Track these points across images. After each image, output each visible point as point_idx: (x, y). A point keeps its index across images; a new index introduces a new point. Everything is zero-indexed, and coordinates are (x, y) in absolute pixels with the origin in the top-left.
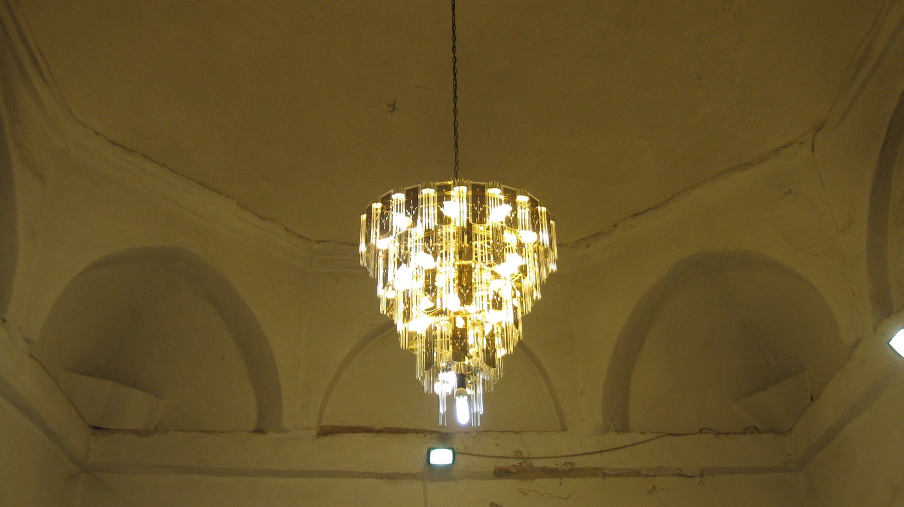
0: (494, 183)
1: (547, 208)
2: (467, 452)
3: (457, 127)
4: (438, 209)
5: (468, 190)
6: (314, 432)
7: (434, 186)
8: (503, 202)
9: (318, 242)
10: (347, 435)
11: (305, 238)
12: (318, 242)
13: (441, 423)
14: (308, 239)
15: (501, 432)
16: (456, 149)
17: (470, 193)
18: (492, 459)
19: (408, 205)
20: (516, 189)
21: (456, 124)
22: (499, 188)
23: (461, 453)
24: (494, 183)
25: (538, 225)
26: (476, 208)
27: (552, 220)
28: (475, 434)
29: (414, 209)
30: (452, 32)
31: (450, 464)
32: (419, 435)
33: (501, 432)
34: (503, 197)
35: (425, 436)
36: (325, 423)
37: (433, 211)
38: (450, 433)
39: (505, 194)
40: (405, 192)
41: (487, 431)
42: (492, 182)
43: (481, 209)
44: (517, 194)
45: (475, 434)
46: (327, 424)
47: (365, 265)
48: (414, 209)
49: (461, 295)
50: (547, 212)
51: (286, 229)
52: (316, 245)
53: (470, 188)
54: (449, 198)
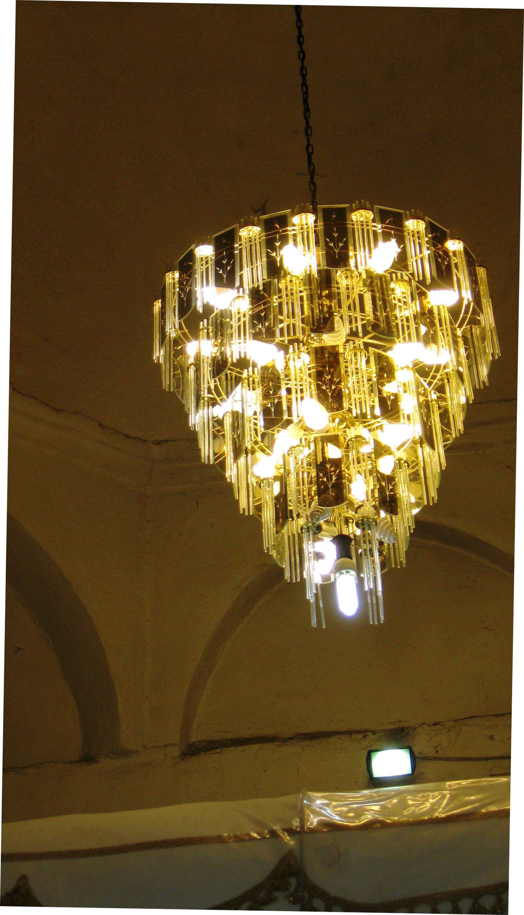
0: (360, 202)
1: (464, 242)
2: (441, 754)
3: (312, 153)
4: (268, 256)
5: (316, 221)
6: (176, 752)
7: (259, 221)
8: (380, 238)
9: (157, 443)
10: (232, 749)
11: (135, 438)
12: (157, 443)
13: (314, 622)
14: (140, 439)
15: (496, 716)
16: (313, 188)
17: (320, 224)
18: (483, 762)
19: (218, 263)
20: (402, 211)
21: (310, 151)
22: (372, 210)
23: (424, 758)
24: (360, 202)
25: (449, 267)
26: (332, 245)
27: (480, 266)
28: (451, 724)
29: (228, 264)
30: (295, 15)
31: (408, 775)
32: (353, 736)
33: (496, 716)
34: (379, 228)
35: (364, 737)
36: (195, 737)
37: (261, 264)
38: (408, 728)
39: (383, 221)
40: (213, 242)
41: (472, 717)
42: (357, 202)
43: (341, 245)
44: (404, 218)
45: (451, 724)
46: (200, 739)
47: (172, 390)
48: (228, 264)
49: (322, 396)
50: (465, 248)
51: (101, 425)
52: (156, 448)
53: (320, 215)
54: (284, 239)
